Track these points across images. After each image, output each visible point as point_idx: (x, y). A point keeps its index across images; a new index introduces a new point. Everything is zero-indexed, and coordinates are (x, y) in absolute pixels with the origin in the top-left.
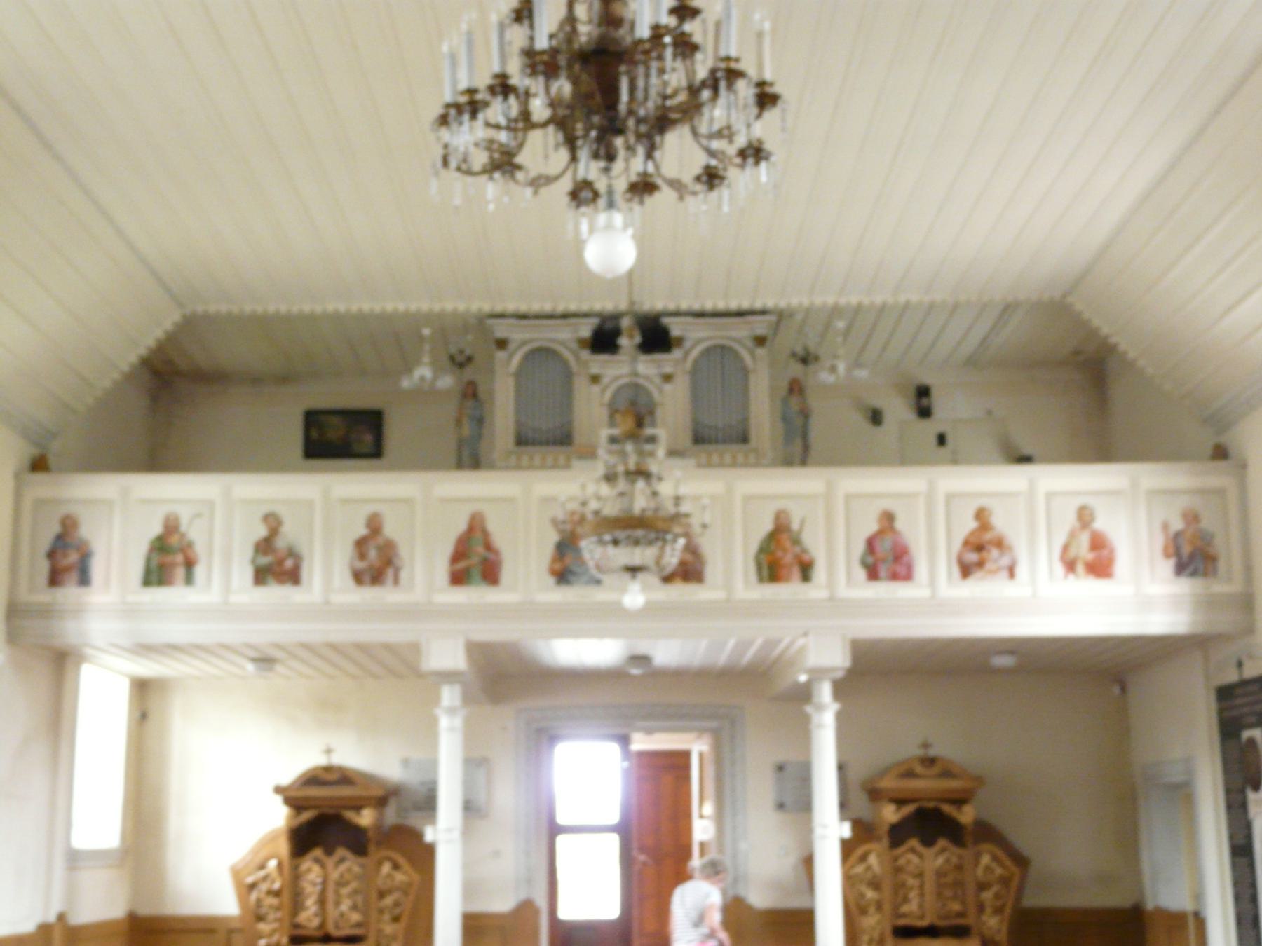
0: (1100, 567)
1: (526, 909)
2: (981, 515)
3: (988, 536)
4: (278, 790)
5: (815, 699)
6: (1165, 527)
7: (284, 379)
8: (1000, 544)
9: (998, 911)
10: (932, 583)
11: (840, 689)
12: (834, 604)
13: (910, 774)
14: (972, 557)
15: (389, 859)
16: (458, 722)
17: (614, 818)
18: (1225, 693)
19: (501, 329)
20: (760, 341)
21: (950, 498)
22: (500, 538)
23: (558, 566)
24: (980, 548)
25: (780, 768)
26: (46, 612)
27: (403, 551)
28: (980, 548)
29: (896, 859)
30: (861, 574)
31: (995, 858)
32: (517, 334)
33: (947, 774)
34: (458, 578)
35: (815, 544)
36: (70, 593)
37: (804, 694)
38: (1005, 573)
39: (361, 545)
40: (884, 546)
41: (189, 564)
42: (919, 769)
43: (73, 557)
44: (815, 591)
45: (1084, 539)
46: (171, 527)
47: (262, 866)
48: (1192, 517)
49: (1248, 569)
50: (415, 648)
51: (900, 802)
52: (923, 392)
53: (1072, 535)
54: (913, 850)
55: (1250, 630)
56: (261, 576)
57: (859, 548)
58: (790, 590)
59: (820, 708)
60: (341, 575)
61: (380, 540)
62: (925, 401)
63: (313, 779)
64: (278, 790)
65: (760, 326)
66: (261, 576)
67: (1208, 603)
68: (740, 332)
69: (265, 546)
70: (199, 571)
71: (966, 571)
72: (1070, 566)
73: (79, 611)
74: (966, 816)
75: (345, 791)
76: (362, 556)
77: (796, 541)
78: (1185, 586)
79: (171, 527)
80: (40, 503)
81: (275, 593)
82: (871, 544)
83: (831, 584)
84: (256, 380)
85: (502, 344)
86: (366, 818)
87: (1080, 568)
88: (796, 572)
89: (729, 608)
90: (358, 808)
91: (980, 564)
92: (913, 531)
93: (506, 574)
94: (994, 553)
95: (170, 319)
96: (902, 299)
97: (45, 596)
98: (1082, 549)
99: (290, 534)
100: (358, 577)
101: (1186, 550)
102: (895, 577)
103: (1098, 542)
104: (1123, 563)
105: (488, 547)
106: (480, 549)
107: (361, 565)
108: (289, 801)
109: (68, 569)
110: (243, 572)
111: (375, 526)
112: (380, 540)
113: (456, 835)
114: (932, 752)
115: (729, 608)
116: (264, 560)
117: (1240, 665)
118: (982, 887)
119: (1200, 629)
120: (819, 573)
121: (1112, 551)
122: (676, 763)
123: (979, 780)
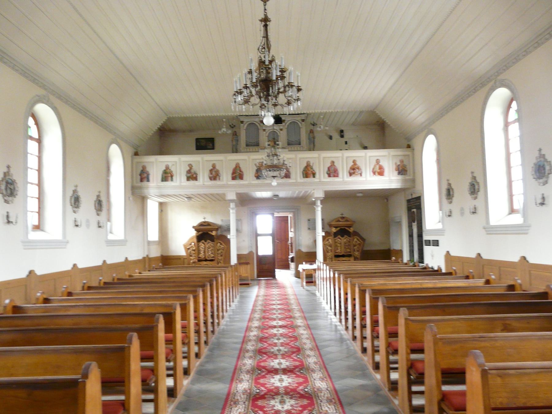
0: (381, 173)
1: (251, 253)
2: (354, 162)
3: (356, 166)
4: (194, 227)
5: (316, 205)
6: (396, 164)
7: (191, 131)
8: (358, 168)
9: (358, 251)
10: (343, 177)
11: (322, 202)
12: (321, 183)
13: (339, 221)
14: (352, 171)
15: (219, 242)
16: (234, 211)
17: (271, 232)
18: (409, 201)
19: (242, 119)
20: (303, 120)
21: (347, 157)
22: (243, 169)
23: (257, 175)
24: (354, 169)
25: (309, 220)
26: (140, 188)
27: (221, 172)
28: (354, 169)
29: (335, 240)
30: (327, 175)
31: (358, 240)
32: (245, 120)
33: (347, 221)
34: (234, 178)
35: (316, 169)
36: (145, 183)
37: (314, 203)
38: (359, 175)
39: (211, 171)
40: (332, 169)
41: (172, 176)
42: (341, 220)
43: (145, 175)
44: (316, 180)
45: (378, 167)
46: (167, 167)
47: (191, 245)
48: (402, 161)
49: (414, 173)
50: (224, 194)
51: (336, 227)
52: (342, 131)
53: (375, 166)
54: (339, 238)
55: (414, 187)
56: (188, 179)
57: (326, 169)
58: (310, 180)
59: (318, 206)
60: (207, 178)
61: (215, 170)
62: (342, 134)
63: (201, 224)
64: (194, 227)
65: (303, 117)
66: (188, 179)
67: (405, 181)
68: (298, 118)
69: (189, 172)
70: (174, 178)
71: (351, 174)
72: (374, 173)
73: (148, 187)
74: (351, 230)
75: (209, 227)
76: (211, 174)
77: (312, 168)
78: (400, 177)
79: (167, 167)
80: (137, 162)
81: (192, 183)
82: (329, 168)
83: (320, 178)
84: (184, 131)
85: (242, 122)
86: (214, 233)
87: (377, 174)
88: (312, 175)
89: (296, 184)
90: (212, 231)
91: (354, 173)
92: (338, 165)
93: (245, 177)
94: (357, 170)
95: (164, 119)
96: (336, 111)
97: (140, 184)
98: (377, 169)
99: (195, 168)
100: (211, 179)
101: (401, 169)
102: (334, 176)
103: (381, 168)
104: (386, 172)
105: (240, 171)
106: (239, 172)
107: (211, 176)
108: (196, 230)
109: (145, 178)
110: (184, 178)
111: (214, 166)
112: (215, 170)
113: (235, 237)
114: (344, 216)
115: (296, 184)
116: (189, 175)
117: (412, 195)
118: (355, 246)
119: (403, 187)
120: (317, 176)
121: (384, 169)
122: (285, 220)
123: (354, 222)
